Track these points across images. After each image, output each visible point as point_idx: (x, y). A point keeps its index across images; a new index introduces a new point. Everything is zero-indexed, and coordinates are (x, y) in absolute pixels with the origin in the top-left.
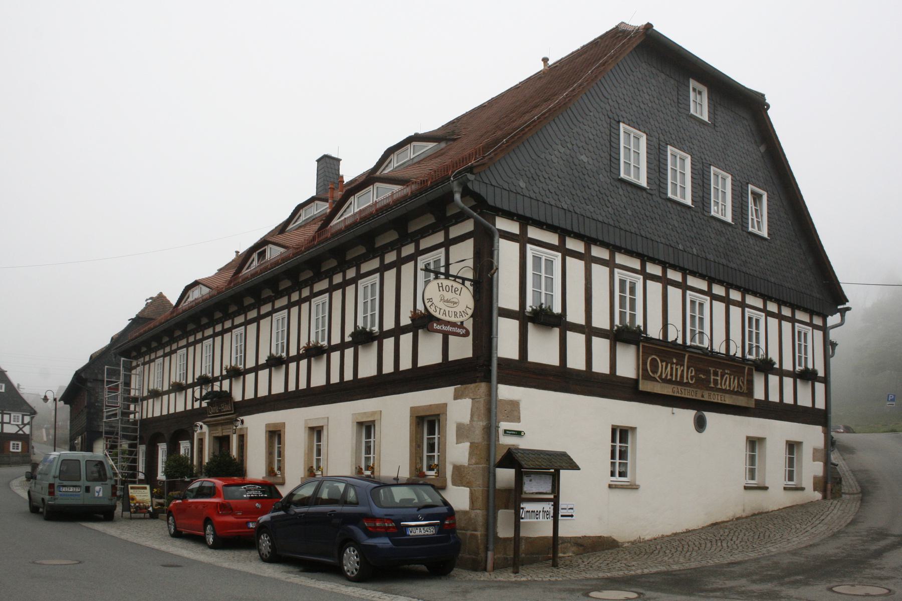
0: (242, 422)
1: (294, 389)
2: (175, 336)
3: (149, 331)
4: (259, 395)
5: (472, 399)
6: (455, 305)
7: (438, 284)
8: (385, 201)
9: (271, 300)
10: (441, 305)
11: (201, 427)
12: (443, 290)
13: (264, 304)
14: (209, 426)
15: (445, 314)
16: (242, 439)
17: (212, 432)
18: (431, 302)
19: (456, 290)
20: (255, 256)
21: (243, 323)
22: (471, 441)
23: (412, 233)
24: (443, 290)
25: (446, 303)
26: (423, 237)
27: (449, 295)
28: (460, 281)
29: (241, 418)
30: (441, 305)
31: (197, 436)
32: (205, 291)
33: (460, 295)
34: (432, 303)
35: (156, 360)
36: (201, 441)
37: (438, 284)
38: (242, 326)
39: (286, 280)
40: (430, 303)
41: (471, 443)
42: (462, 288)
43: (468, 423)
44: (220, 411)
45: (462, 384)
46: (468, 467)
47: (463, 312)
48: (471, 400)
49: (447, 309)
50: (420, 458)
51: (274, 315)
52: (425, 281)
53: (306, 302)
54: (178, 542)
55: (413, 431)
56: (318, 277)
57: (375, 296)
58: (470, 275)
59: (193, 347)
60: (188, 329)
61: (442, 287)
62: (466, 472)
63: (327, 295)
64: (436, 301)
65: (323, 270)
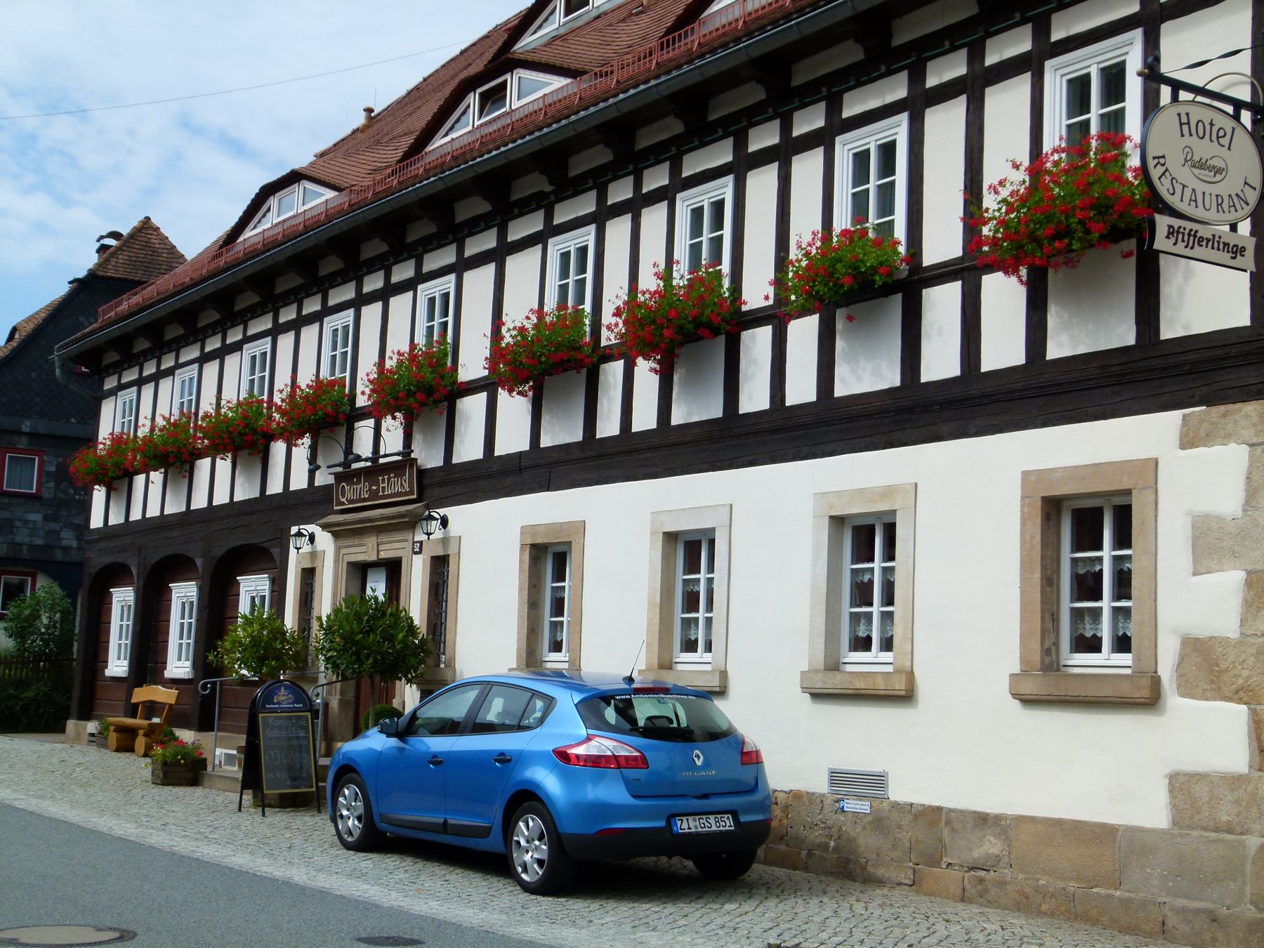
0: (444, 522)
1: (139, 517)
2: (135, 351)
3: (117, 322)
4: (499, 451)
5: (1251, 445)
6: (1218, 177)
7: (1179, 115)
8: (531, 106)
9: (545, 203)
10: (1185, 175)
11: (312, 538)
12: (1191, 135)
13: (804, 105)
14: (336, 535)
15: (1196, 201)
16: (440, 567)
17: (344, 551)
18: (1163, 165)
19: (1221, 133)
20: (473, 100)
21: (453, 265)
22: (1250, 568)
23: (323, 276)
24: (1191, 135)
25: (1197, 171)
26: (471, 234)
27: (1205, 149)
28: (1229, 109)
29: (442, 511)
30: (1185, 175)
31: (298, 562)
32: (323, 197)
33: (1229, 149)
34: (1163, 169)
35: (177, 372)
36: (309, 575)
37: (1179, 115)
38: (347, 308)
39: (377, 241)
40: (1160, 169)
41: (1249, 573)
42: (1234, 129)
43: (1239, 513)
44: (374, 495)
45: (1209, 401)
46: (1240, 643)
47: (1237, 195)
48: (1245, 449)
49: (1201, 187)
50: (1053, 615)
51: (420, 287)
52: (854, 194)
53: (213, 358)
54: (367, 862)
55: (1032, 537)
56: (701, 135)
57: (1089, 112)
58: (1244, 94)
59: (291, 335)
60: (167, 337)
61: (1188, 123)
62: (1231, 658)
63: (351, 312)
64: (1175, 163)
65: (515, 197)
